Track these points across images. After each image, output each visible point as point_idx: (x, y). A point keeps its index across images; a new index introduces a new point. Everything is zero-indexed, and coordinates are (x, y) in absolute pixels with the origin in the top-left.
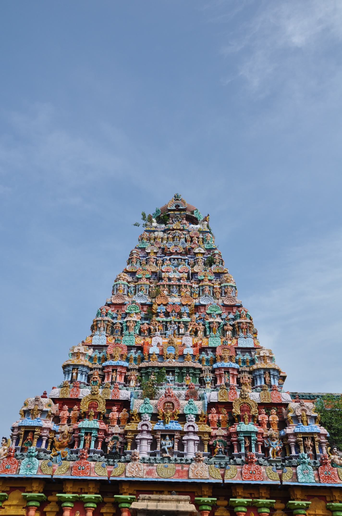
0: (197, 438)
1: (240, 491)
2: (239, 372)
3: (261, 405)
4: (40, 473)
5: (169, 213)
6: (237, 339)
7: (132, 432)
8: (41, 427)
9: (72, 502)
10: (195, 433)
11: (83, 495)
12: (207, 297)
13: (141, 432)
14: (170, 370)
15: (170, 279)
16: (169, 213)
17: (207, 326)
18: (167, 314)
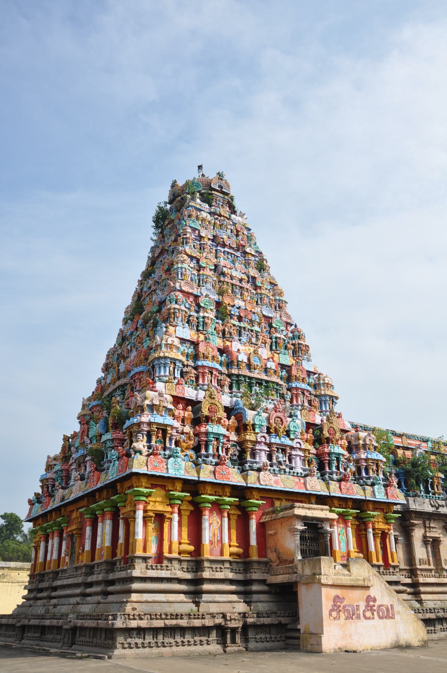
2: (184, 365)
4: (186, 474)
5: (213, 192)
6: (231, 342)
8: (172, 426)
10: (300, 449)
11: (224, 498)
12: (268, 308)
13: (260, 443)
14: (260, 382)
15: (232, 278)
16: (213, 192)
17: (274, 340)
18: (240, 319)
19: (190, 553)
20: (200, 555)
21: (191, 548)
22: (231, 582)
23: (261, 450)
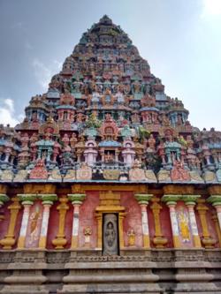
0: (95, 151)
1: (171, 189)
3: (180, 134)
7: (82, 148)
9: (31, 200)
10: (132, 149)
19: (165, 245)
20: (173, 246)
21: (165, 241)
22: (208, 270)
23: (127, 154)
